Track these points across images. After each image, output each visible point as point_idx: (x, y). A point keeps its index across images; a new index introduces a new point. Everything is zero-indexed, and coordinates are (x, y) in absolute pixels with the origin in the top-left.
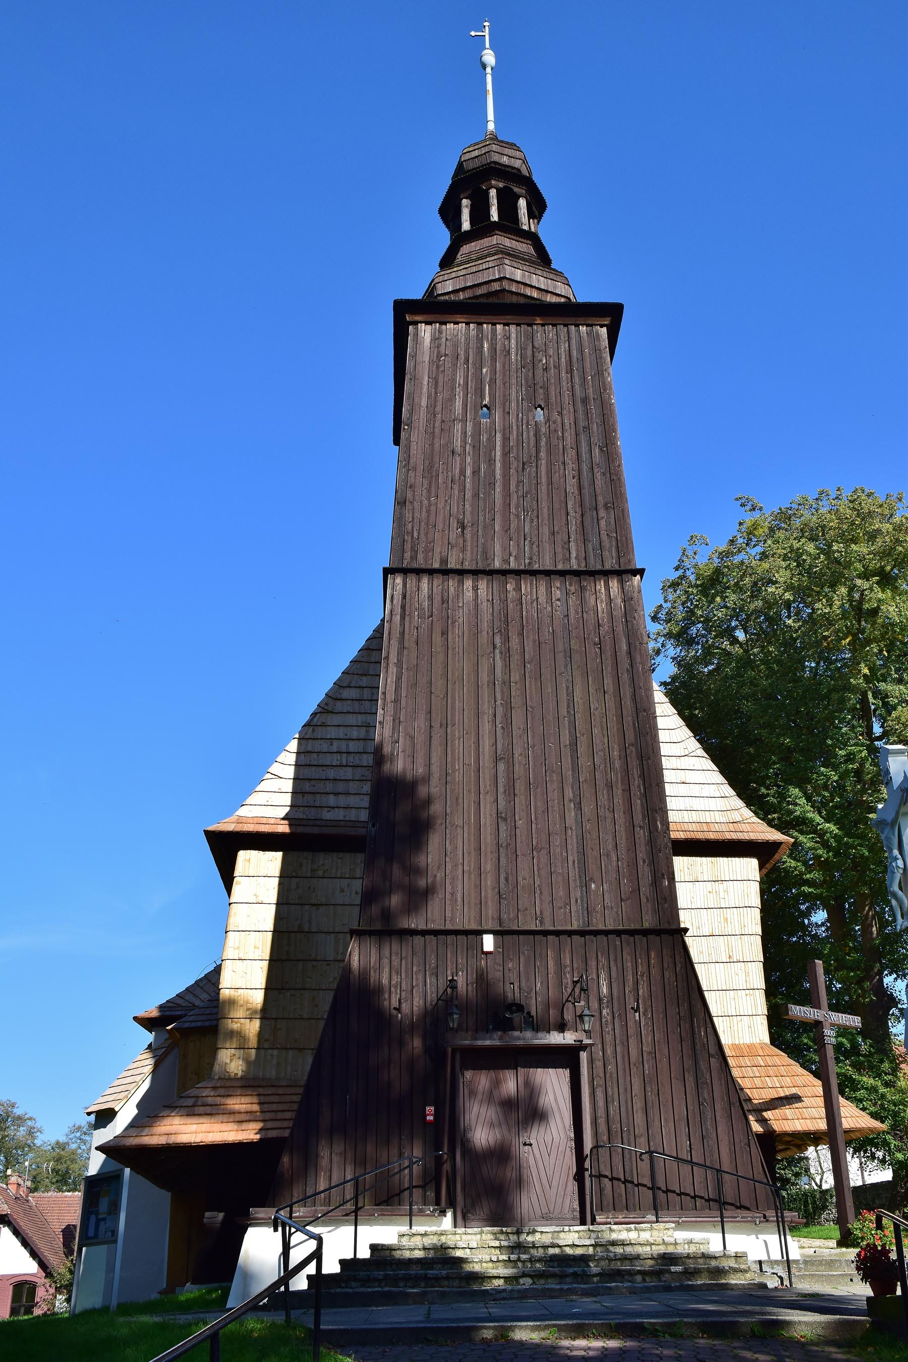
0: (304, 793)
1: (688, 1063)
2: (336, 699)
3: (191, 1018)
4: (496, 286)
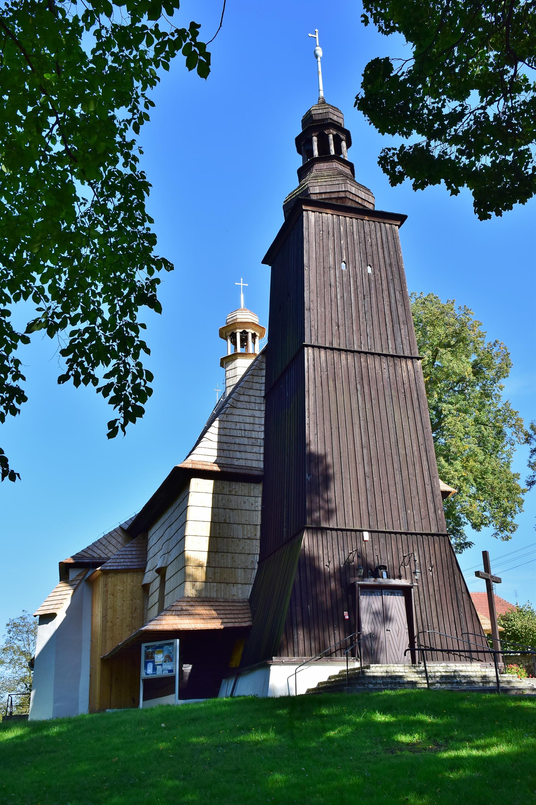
0: (224, 450)
1: (454, 596)
2: (237, 401)
3: (109, 564)
4: (342, 195)
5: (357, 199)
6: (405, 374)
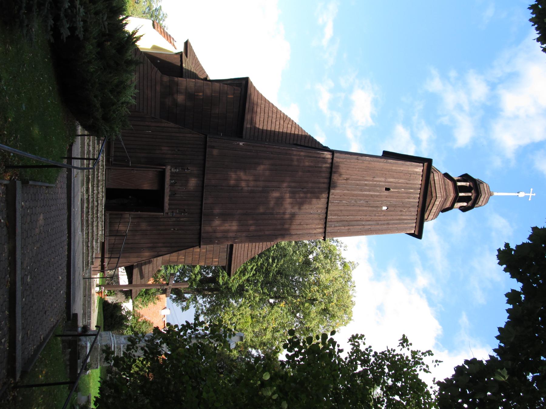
4: (434, 195)
5: (431, 206)
6: (313, 226)
